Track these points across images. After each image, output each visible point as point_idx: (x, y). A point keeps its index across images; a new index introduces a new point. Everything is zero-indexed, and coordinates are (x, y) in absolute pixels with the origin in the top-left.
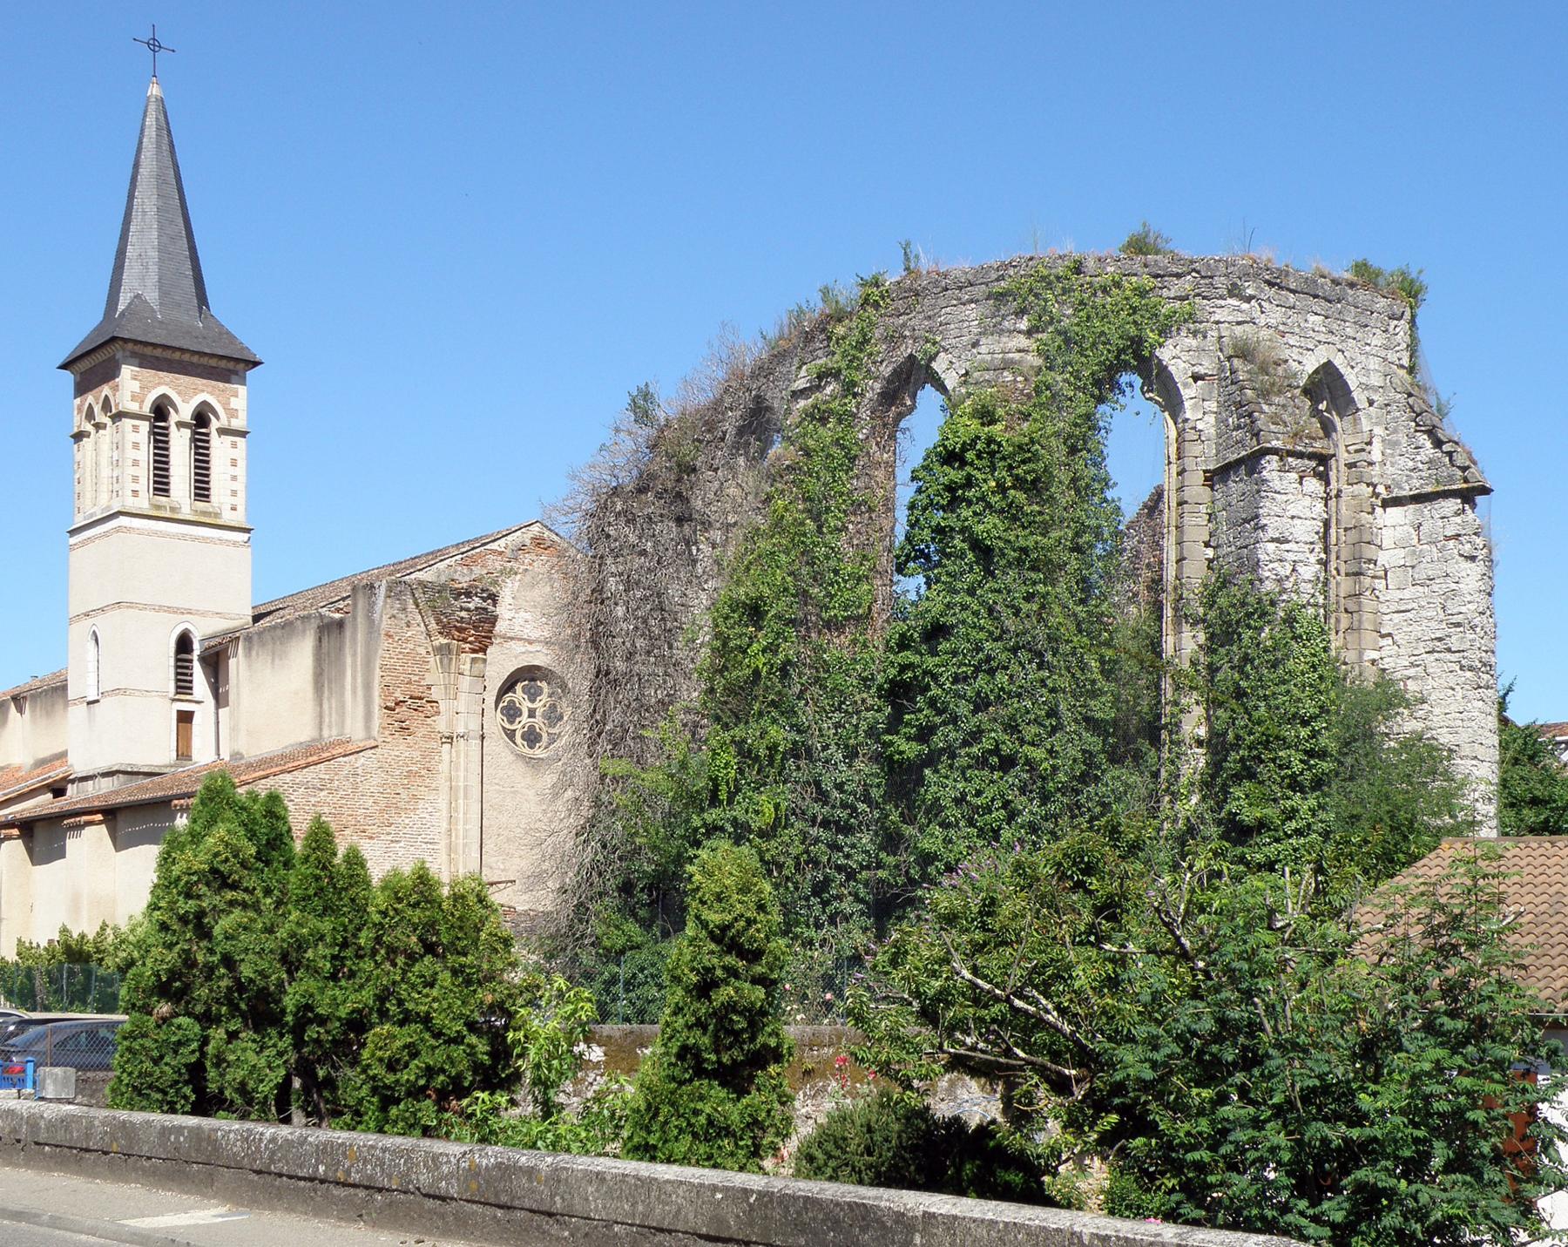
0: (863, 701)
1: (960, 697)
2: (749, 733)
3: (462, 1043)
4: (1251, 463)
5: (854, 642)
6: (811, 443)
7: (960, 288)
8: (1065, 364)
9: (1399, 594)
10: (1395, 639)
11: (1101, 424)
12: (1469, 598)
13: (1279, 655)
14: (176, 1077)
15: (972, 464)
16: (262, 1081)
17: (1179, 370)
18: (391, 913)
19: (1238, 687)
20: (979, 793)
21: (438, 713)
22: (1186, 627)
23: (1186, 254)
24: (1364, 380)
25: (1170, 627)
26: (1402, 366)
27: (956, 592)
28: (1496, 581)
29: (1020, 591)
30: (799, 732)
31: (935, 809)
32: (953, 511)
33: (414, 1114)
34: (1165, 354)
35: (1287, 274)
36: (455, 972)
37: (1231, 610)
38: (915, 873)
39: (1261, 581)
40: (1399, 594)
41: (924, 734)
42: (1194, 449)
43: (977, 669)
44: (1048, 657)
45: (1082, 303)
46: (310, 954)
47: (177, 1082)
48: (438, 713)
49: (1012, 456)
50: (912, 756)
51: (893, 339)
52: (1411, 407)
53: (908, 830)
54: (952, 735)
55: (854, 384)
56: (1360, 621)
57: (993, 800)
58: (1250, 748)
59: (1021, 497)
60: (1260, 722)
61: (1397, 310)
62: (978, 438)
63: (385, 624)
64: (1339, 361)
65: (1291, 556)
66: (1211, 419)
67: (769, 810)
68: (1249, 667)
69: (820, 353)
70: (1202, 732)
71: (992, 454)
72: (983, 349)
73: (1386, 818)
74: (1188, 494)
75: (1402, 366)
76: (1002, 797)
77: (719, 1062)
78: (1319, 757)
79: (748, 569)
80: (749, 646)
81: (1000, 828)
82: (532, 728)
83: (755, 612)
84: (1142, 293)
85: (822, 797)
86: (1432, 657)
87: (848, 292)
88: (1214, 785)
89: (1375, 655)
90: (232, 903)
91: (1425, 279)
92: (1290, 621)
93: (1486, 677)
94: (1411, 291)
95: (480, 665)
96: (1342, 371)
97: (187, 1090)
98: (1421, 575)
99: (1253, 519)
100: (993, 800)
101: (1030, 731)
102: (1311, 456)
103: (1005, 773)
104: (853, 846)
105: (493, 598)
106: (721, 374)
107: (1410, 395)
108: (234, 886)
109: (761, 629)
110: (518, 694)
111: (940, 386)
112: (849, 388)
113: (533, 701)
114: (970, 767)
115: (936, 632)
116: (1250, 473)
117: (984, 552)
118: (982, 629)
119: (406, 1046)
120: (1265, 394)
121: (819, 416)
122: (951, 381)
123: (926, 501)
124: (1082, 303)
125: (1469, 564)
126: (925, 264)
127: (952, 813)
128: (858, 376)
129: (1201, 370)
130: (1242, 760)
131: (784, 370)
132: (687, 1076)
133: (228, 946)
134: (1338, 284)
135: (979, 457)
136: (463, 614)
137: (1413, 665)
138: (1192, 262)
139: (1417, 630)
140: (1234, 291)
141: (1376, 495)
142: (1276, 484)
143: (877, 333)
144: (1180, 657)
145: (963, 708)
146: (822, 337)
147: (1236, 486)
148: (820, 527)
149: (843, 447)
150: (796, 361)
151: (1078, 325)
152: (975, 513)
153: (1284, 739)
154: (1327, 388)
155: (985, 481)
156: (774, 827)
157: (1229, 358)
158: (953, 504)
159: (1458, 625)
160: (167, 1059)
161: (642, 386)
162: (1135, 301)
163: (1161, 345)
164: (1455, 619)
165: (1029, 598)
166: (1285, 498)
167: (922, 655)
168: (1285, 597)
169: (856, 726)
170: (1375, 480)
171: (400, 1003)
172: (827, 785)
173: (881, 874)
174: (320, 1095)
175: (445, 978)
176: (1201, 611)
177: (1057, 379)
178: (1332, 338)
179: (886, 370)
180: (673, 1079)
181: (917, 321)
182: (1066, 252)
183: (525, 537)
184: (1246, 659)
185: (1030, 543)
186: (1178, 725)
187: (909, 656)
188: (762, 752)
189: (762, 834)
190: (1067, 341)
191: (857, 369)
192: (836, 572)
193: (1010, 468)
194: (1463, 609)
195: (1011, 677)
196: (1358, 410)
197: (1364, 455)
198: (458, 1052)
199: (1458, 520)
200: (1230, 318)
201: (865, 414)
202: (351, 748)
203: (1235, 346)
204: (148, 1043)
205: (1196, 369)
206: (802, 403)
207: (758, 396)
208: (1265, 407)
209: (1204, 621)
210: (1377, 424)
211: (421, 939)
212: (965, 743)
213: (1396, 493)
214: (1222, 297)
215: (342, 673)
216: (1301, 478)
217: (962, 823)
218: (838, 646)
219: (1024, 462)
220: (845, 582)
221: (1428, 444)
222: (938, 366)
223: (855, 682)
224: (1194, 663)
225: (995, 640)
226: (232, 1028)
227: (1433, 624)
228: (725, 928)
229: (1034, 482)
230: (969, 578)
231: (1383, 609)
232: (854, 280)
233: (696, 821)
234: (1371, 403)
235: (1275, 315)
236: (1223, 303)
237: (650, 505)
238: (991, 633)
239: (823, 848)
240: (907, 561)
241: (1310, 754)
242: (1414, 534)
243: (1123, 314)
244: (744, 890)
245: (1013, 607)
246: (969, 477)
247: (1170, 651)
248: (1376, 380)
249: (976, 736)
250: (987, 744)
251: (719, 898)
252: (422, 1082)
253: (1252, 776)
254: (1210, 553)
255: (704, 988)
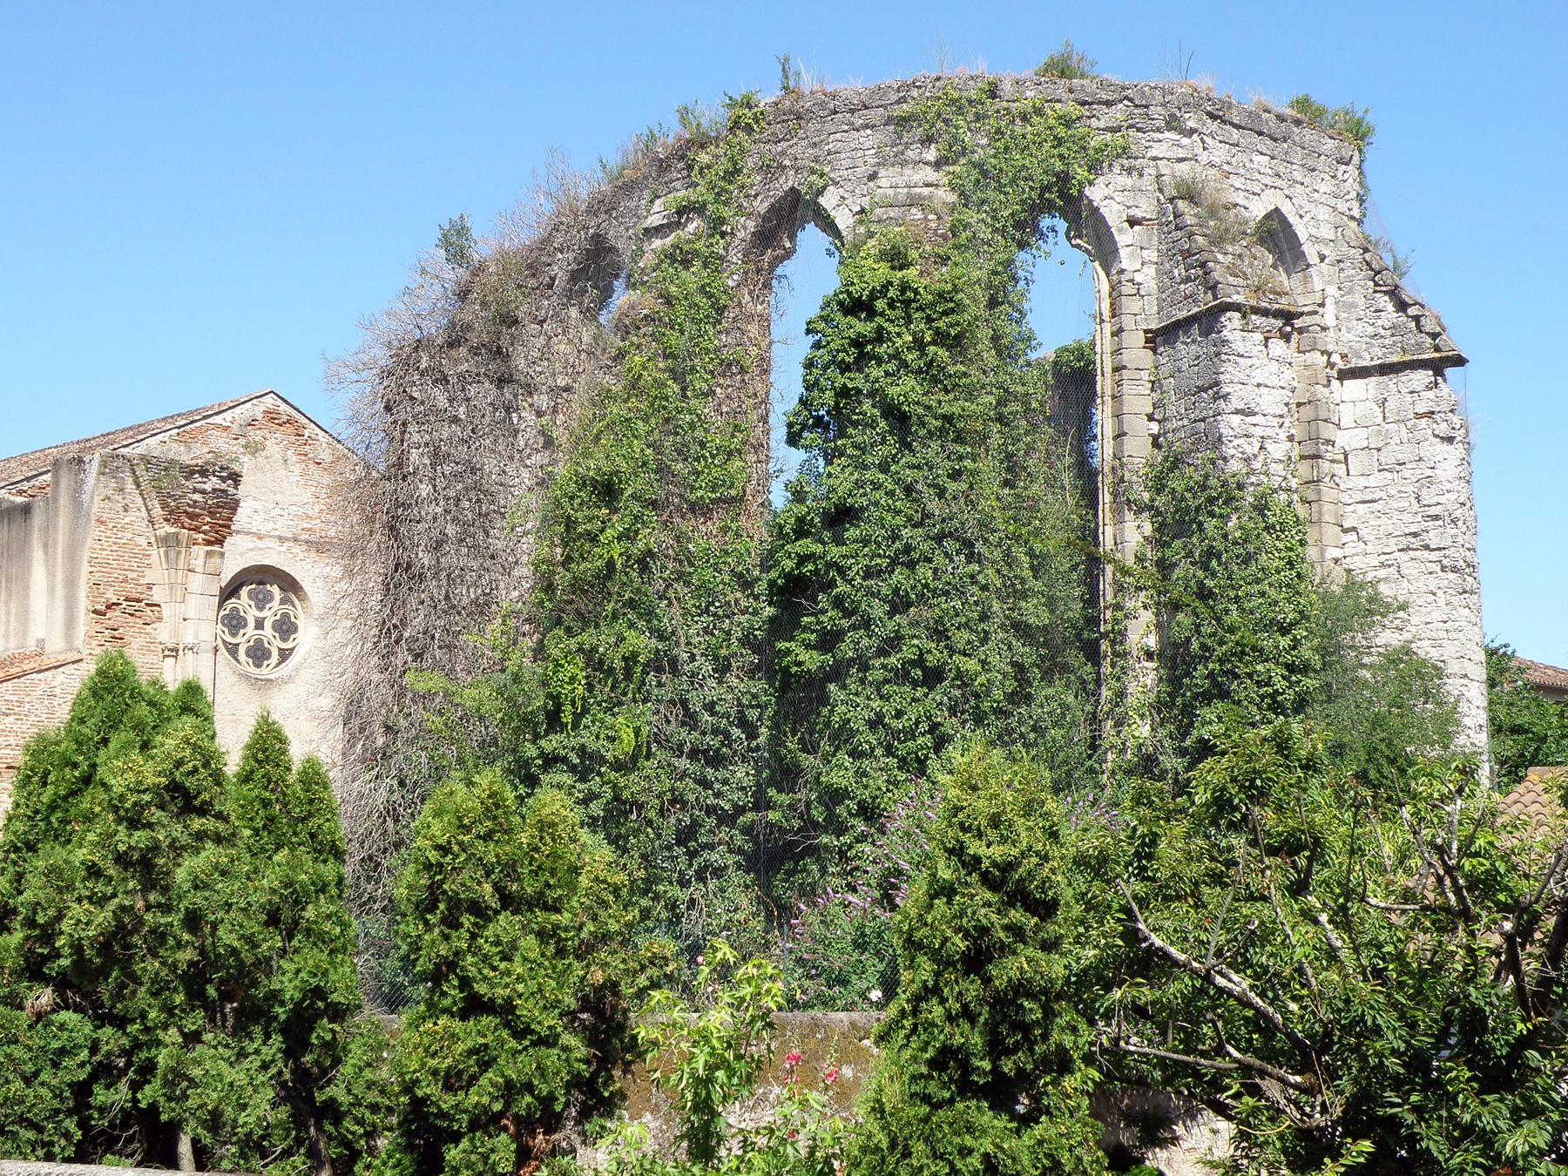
0: (737, 601)
1: (873, 595)
2: (601, 639)
3: (554, 1045)
4: (1208, 321)
5: (725, 530)
6: (673, 289)
7: (852, 111)
8: (983, 202)
9: (1363, 482)
10: (1355, 539)
11: (1021, 274)
12: (1448, 486)
13: (1251, 548)
14: (56, 1104)
15: (882, 314)
16: (244, 1107)
17: (1113, 214)
18: (456, 848)
19: (1201, 584)
20: (899, 714)
21: (160, 619)
22: (1129, 516)
23: (1117, 79)
24: (1314, 232)
25: (1108, 515)
26: (1352, 218)
27: (866, 467)
28: (1474, 468)
29: (944, 467)
30: (661, 638)
31: (842, 735)
32: (860, 370)
33: (485, 1158)
34: (1095, 194)
35: (1230, 108)
36: (541, 935)
37: (1188, 495)
38: (818, 814)
39: (1225, 459)
40: (1363, 482)
41: (828, 640)
42: (1131, 305)
43: (894, 562)
44: (979, 547)
45: (998, 131)
46: (310, 913)
47: (57, 1112)
48: (160, 619)
49: (933, 305)
50: (813, 668)
51: (771, 170)
52: (1368, 264)
53: (807, 761)
54: (865, 642)
55: (722, 221)
56: (1320, 512)
57: (917, 723)
58: (1221, 661)
59: (943, 354)
60: (1232, 630)
61: (1346, 153)
62: (890, 283)
63: (97, 507)
64: (1287, 209)
65: (1258, 432)
66: (1151, 271)
67: (627, 736)
68: (1214, 563)
69: (678, 184)
70: (1152, 642)
71: (907, 303)
72: (883, 182)
73: (1383, 747)
74: (1127, 358)
75: (1352, 218)
76: (929, 718)
77: (996, 1070)
78: (1300, 672)
79: (597, 438)
80: (602, 531)
81: (927, 758)
82: (259, 642)
83: (607, 491)
84: (1068, 123)
85: (690, 720)
86: (1405, 556)
87: (712, 113)
88: (1175, 706)
89: (1338, 553)
90: (200, 836)
91: (1370, 118)
92: (1261, 508)
93: (1469, 579)
94: (1359, 133)
95: (216, 560)
96: (1291, 220)
97: (71, 1124)
98: (1388, 457)
99: (1213, 388)
100: (917, 723)
101: (961, 638)
102: (1278, 314)
103: (931, 689)
104: (725, 782)
105: (235, 478)
106: (548, 207)
107: (1366, 250)
108: (202, 811)
109: (616, 510)
110: (244, 601)
111: (829, 226)
112: (716, 226)
113: (261, 609)
114: (886, 681)
115: (841, 516)
116: (1206, 333)
117: (898, 418)
118: (898, 512)
119: (471, 1052)
120: (1218, 241)
121: (681, 258)
122: (844, 220)
123: (827, 358)
124: (998, 131)
125: (1446, 447)
126: (807, 83)
127: (867, 739)
128: (726, 212)
129: (1139, 214)
130: (1211, 676)
131: (632, 204)
132: (947, 1095)
133: (198, 899)
134: (1283, 120)
135: (891, 305)
136: (197, 497)
137: (1383, 565)
138: (1123, 88)
139: (1386, 524)
140: (1173, 123)
141: (1331, 365)
142: (1239, 346)
143: (750, 162)
144: (1122, 551)
145: (878, 610)
146: (681, 165)
147: (1187, 349)
148: (684, 389)
149: (709, 296)
150: (647, 195)
151: (995, 156)
152: (887, 374)
153: (1261, 651)
154: (1277, 236)
155: (899, 335)
156: (634, 758)
157: (1172, 200)
158: (862, 360)
159: (1436, 518)
160: (44, 1077)
161: (456, 218)
162: (1061, 131)
163: (1091, 183)
164: (1433, 511)
165: (955, 475)
166: (1249, 362)
167: (824, 543)
168: (1253, 479)
169: (728, 633)
170: (1330, 348)
171: (465, 983)
172: (696, 706)
173: (773, 816)
174: (320, 1129)
175: (530, 943)
176: (1146, 496)
177: (972, 216)
178: (1279, 183)
179: (762, 206)
180: (926, 1099)
181: (800, 149)
182: (978, 72)
183: (257, 410)
184: (1211, 553)
185: (956, 410)
186: (1123, 634)
187: (807, 545)
188: (618, 664)
189: (618, 766)
190: (985, 174)
191: (726, 204)
192: (702, 445)
193: (929, 320)
194: (1442, 499)
195: (935, 571)
196: (1309, 266)
197: (1316, 319)
198: (552, 1057)
199: (1431, 394)
200: (1169, 154)
201: (735, 257)
202: (47, 661)
203: (1178, 186)
204: (18, 1052)
205: (1132, 212)
206: (657, 243)
207: (597, 235)
208: (1220, 257)
209: (1150, 508)
210: (1329, 283)
211: (497, 888)
212: (882, 652)
213: (1355, 363)
214: (1159, 130)
215: (26, 569)
216: (1267, 339)
217: (879, 752)
218: (703, 535)
219: (945, 313)
220: (713, 456)
221: (1390, 307)
222: (828, 201)
223: (727, 578)
224: (1140, 559)
225: (915, 526)
226: (191, 1028)
227: (1406, 517)
228: (1008, 867)
229: (957, 337)
230: (883, 451)
231: (1345, 498)
232: (720, 101)
233: (530, 751)
234: (1322, 258)
235: (1219, 153)
236: (1160, 136)
237: (462, 363)
238: (910, 519)
239: (692, 785)
240: (802, 430)
241: (1291, 668)
242: (1378, 412)
243: (1047, 146)
244: (1028, 809)
245: (935, 486)
246: (880, 330)
247: (1109, 544)
248: (1327, 232)
249: (892, 644)
250: (908, 653)
251: (995, 822)
252: (497, 1107)
253: (1224, 695)
254: (1155, 428)
255: (976, 961)
